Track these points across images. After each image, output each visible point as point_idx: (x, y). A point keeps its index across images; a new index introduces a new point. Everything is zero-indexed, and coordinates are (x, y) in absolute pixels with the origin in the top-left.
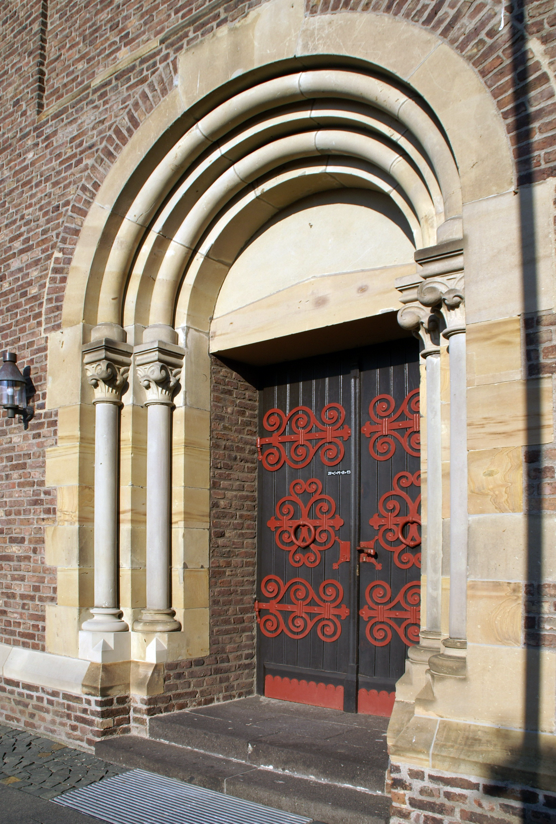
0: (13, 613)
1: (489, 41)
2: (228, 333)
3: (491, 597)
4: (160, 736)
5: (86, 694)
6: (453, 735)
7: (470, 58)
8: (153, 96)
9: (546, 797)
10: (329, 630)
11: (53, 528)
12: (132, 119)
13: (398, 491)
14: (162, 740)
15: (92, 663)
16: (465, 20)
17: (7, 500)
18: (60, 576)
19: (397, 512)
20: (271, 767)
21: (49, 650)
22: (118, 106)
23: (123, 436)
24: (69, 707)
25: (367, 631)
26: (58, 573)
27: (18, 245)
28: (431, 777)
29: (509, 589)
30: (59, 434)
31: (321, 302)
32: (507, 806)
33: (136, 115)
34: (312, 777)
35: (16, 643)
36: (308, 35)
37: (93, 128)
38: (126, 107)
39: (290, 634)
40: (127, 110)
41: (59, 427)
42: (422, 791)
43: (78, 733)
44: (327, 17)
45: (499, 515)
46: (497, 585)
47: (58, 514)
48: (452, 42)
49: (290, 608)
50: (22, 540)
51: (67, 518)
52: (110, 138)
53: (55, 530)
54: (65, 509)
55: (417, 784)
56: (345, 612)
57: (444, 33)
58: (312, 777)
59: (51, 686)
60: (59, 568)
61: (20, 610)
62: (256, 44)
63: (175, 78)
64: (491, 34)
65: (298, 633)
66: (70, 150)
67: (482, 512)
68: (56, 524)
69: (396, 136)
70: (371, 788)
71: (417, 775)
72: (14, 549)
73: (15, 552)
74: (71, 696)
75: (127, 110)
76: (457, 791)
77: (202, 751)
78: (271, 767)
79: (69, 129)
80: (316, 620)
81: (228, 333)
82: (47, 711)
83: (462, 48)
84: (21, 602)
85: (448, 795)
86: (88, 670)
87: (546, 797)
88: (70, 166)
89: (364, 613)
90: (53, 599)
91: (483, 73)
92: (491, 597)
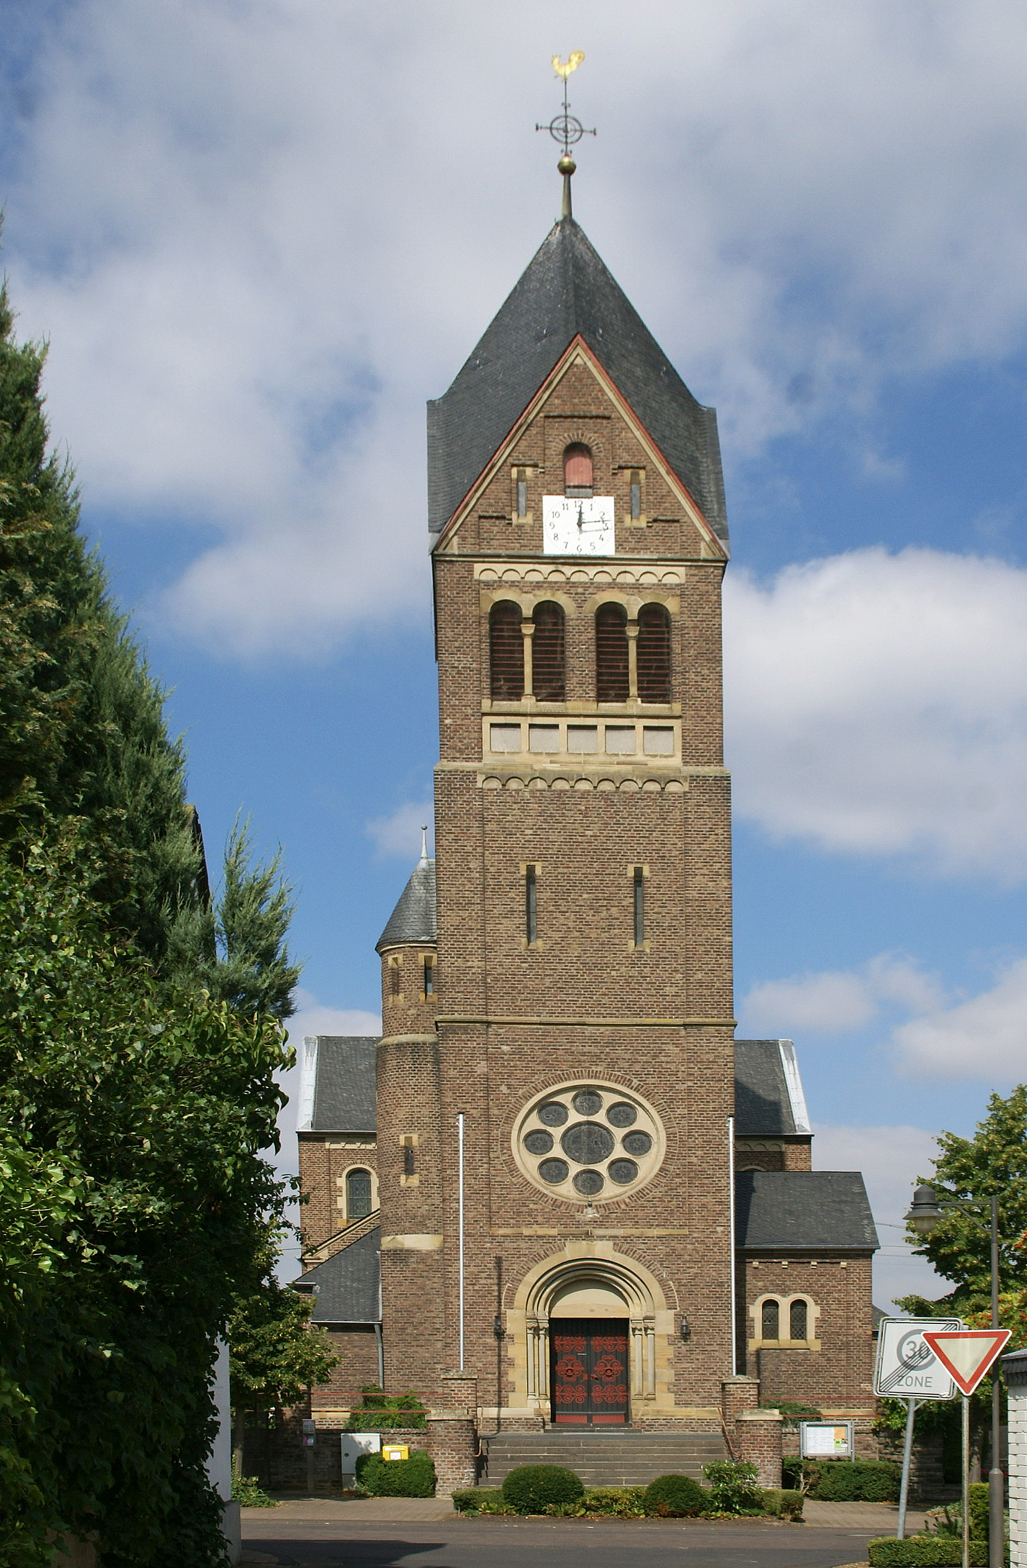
27: (483, 1275)
31: (592, 1311)
59: (517, 1417)
89: (593, 1394)
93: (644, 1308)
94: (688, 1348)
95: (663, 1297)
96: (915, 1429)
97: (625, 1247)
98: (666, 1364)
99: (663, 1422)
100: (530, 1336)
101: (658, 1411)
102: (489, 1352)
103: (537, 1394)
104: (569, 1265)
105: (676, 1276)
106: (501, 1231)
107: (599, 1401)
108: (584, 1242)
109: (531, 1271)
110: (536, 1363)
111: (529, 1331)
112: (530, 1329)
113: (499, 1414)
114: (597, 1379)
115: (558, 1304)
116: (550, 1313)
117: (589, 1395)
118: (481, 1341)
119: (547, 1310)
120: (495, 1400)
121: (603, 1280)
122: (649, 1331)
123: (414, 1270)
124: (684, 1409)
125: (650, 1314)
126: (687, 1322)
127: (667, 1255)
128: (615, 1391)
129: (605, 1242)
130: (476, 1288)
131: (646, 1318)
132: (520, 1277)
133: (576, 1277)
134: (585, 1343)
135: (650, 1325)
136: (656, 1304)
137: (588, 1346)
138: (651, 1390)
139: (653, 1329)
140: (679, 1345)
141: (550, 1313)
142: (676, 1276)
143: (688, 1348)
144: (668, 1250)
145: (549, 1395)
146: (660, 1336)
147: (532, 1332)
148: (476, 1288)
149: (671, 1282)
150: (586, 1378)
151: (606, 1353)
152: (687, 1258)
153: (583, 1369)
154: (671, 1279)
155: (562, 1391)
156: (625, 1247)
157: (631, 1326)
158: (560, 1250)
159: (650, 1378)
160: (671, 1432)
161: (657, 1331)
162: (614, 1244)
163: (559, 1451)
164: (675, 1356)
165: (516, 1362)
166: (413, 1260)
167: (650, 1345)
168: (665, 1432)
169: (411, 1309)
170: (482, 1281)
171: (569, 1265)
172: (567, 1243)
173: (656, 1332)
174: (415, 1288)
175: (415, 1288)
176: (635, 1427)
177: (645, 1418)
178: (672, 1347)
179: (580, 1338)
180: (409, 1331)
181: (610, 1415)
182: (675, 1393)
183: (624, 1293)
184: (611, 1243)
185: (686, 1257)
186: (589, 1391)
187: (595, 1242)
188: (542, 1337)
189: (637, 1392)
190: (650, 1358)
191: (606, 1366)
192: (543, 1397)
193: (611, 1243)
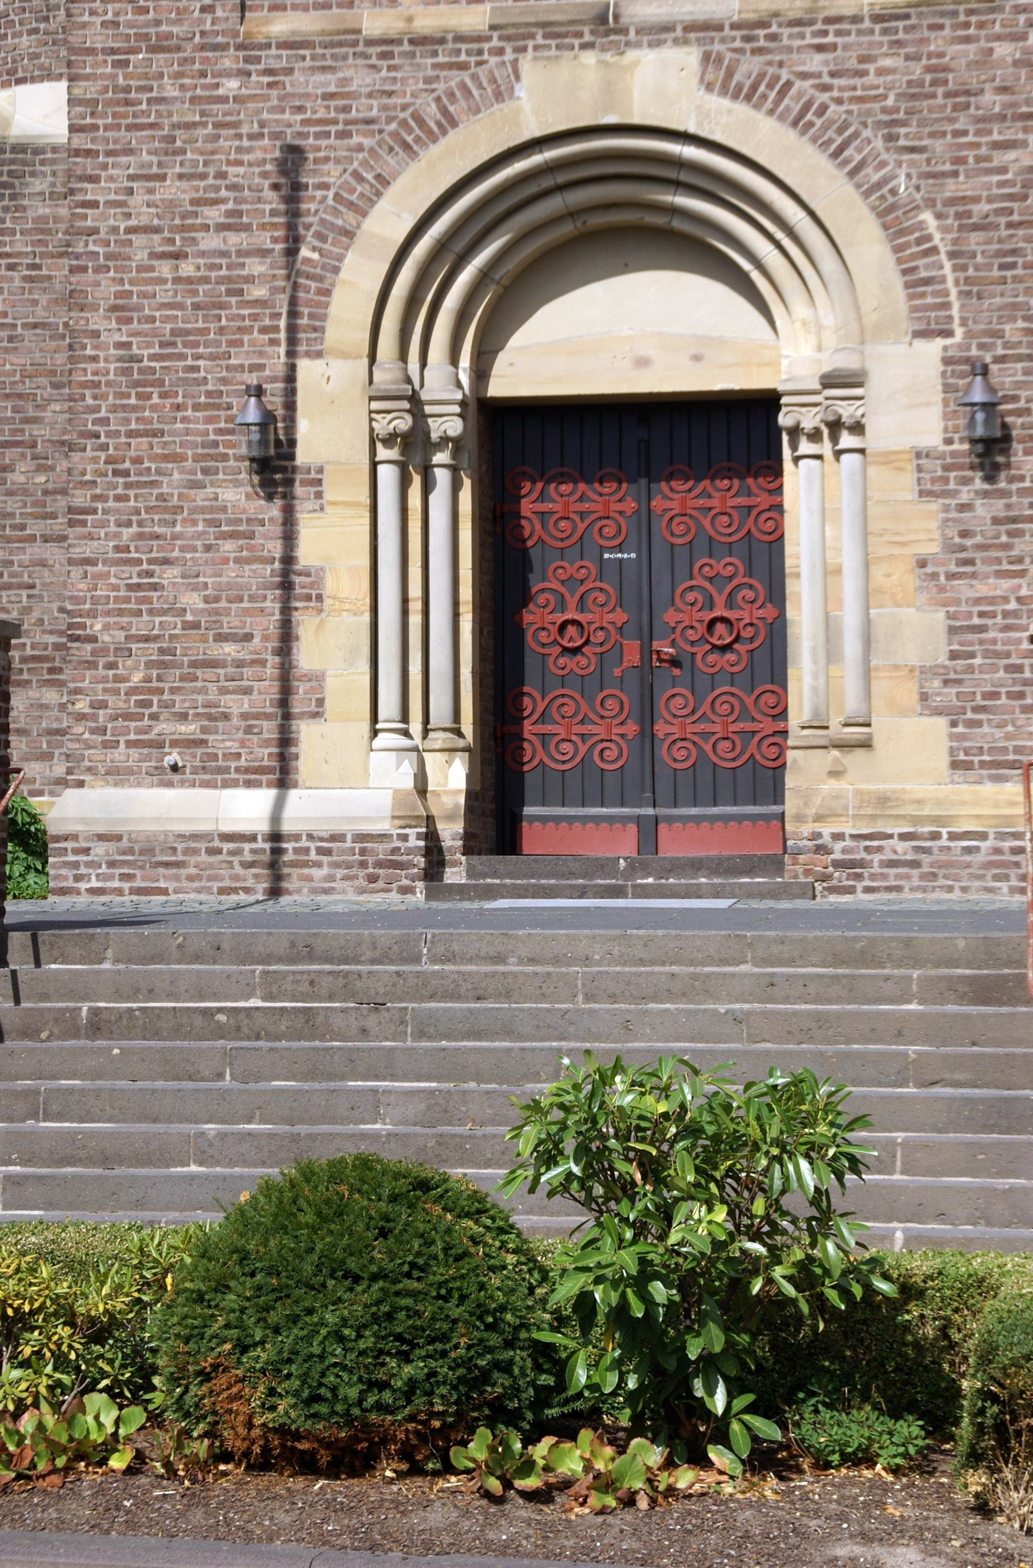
0: (223, 740)
1: (891, 200)
2: (505, 376)
3: (891, 677)
4: (485, 876)
5: (401, 827)
6: (866, 798)
7: (873, 208)
8: (481, 96)
9: (949, 833)
10: (611, 754)
11: (318, 620)
12: (445, 112)
13: (555, 585)
14: (489, 881)
15: (396, 791)
16: (869, 170)
17: (210, 580)
18: (331, 684)
19: (699, 606)
20: (650, 880)
21: (308, 784)
22: (417, 83)
23: (461, 508)
24: (363, 852)
25: (664, 751)
26: (328, 679)
27: (213, 215)
28: (852, 836)
29: (906, 670)
30: (328, 496)
31: (643, 362)
32: (918, 847)
33: (452, 109)
34: (703, 880)
35: (227, 784)
36: (704, 115)
37: (370, 95)
38: (433, 91)
39: (553, 765)
40: (434, 95)
41: (325, 487)
42: (844, 851)
43: (380, 884)
44: (726, 103)
45: (896, 610)
46: (896, 667)
47: (328, 602)
48: (858, 186)
49: (550, 728)
50: (248, 637)
51: (347, 606)
52: (404, 123)
53: (322, 622)
54: (343, 595)
55: (839, 846)
56: (631, 728)
57: (852, 174)
58: (703, 880)
59: (324, 828)
60: (328, 673)
61: (240, 735)
62: (636, 94)
63: (517, 87)
64: (894, 192)
65: (564, 762)
66: (323, 110)
67: (881, 607)
68: (324, 615)
69: (779, 235)
70: (769, 877)
71: (838, 837)
72: (227, 650)
73: (229, 654)
74: (368, 835)
75: (434, 95)
76: (875, 843)
77: (553, 881)
78: (650, 880)
79: (320, 77)
80: (590, 743)
81: (505, 376)
82: (318, 865)
83: (867, 194)
84: (243, 724)
85: (867, 849)
86: (394, 799)
87: (949, 833)
88: (327, 135)
89: (661, 729)
90: (316, 715)
91: (886, 227)
92: (891, 677)
93: (830, 340)
94: (998, 508)
95: (897, 282)
96: (640, 807)
97: (749, 66)
98: (912, 581)
99: (904, 850)
100: (387, 475)
101: (883, 800)
102: (228, 547)
103: (416, 727)
104: (536, 159)
105: (951, 188)
106: (281, 26)
107: (682, 757)
108: (589, 58)
109: (390, 193)
110: (415, 590)
111: (383, 453)
112: (389, 441)
113: (276, 817)
114: (675, 662)
115: (518, 340)
116: (481, 373)
117: (648, 736)
118: (200, 497)
119: (465, 361)
120: (266, 755)
121: (677, 224)
122: (847, 440)
123: (43, 228)
124: (988, 788)
125: (847, 362)
126: (991, 389)
127: (914, 93)
128: (744, 714)
129: (671, 54)
130: (187, 269)
131: (829, 381)
132: (350, 218)
133: (572, 214)
134: (630, 505)
135: (847, 411)
136: (870, 319)
137: (646, 519)
138: (852, 703)
139: (858, 428)
140: (964, 497)
141: (481, 373)
142: (951, 188)
143: (998, 508)
144: (917, 70)
145: (467, 726)
146: (887, 458)
147: (393, 454)
148: (187, 269)
149: (927, 217)
150: (633, 656)
151: (712, 548)
152: (992, 101)
153: (620, 616)
154: (931, 203)
155: (543, 718)
156: (749, 66)
157: (784, 420)
158: (499, 96)
159: (851, 647)
160: (938, 898)
161: (875, 439)
162: (706, 57)
163: (313, 987)
164: (950, 548)
165: (329, 588)
166: (39, 185)
167: (848, 499)
168: (910, 898)
169: (27, 387)
170: (210, 242)
171: (536, 159)
172: (526, 63)
173: (872, 441)
174: (44, 299)
175: (44, 299)
176: (794, 871)
177: (827, 830)
178: (934, 506)
179: (608, 488)
180: (17, 478)
181: (726, 818)
182: (954, 716)
183: (756, 276)
184: (690, 57)
185: (988, 97)
186: (648, 715)
187: (631, 55)
188: (442, 477)
189: (806, 717)
190: (850, 559)
191: (711, 605)
192: (438, 739)
193: (690, 57)
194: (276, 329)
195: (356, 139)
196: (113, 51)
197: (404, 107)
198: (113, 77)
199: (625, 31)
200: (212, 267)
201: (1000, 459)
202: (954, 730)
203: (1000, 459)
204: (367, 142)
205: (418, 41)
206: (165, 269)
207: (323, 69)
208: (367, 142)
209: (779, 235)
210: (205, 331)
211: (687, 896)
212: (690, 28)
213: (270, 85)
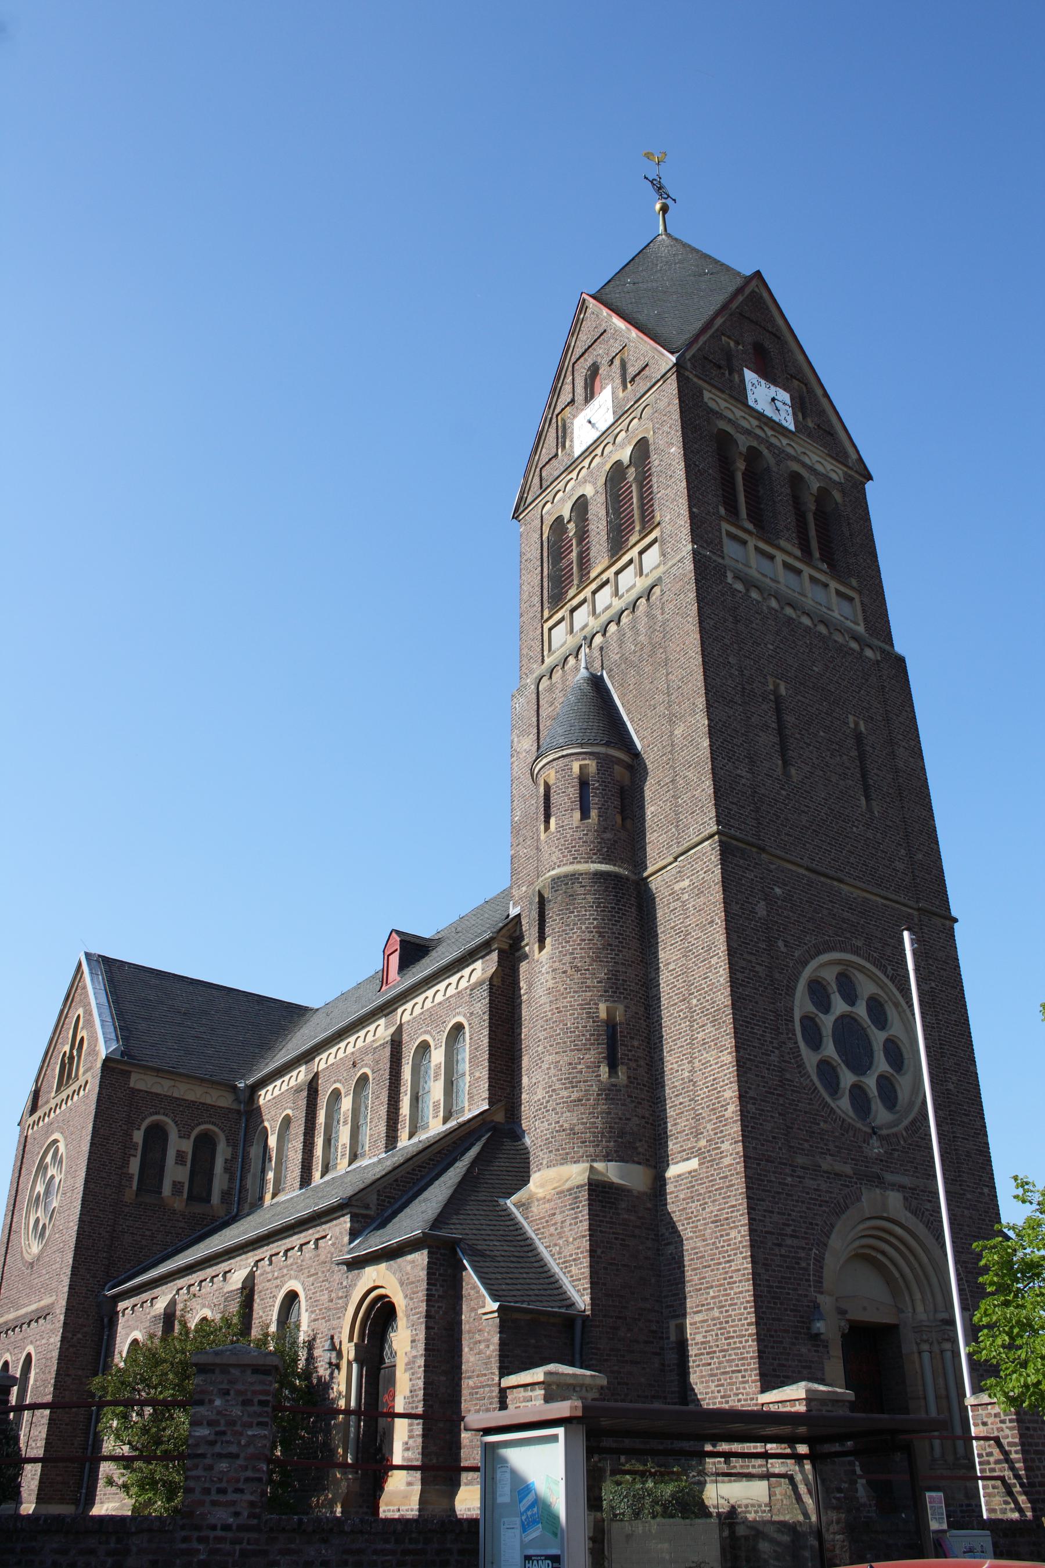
27: (789, 1230)
194: (691, 1324)
195: (824, 1208)
196: (756, 1159)
197: (835, 1198)
198: (757, 1169)
199: (884, 1183)
200: (790, 1252)
201: (608, 835)
202: (987, 1491)
203: (608, 835)
204: (827, 1210)
205: (836, 1174)
206: (777, 1250)
207: (812, 1179)
208: (827, 1210)
209: (912, 1259)
210: (790, 1278)
211: (875, 974)
212: (900, 1186)
213: (800, 1182)
